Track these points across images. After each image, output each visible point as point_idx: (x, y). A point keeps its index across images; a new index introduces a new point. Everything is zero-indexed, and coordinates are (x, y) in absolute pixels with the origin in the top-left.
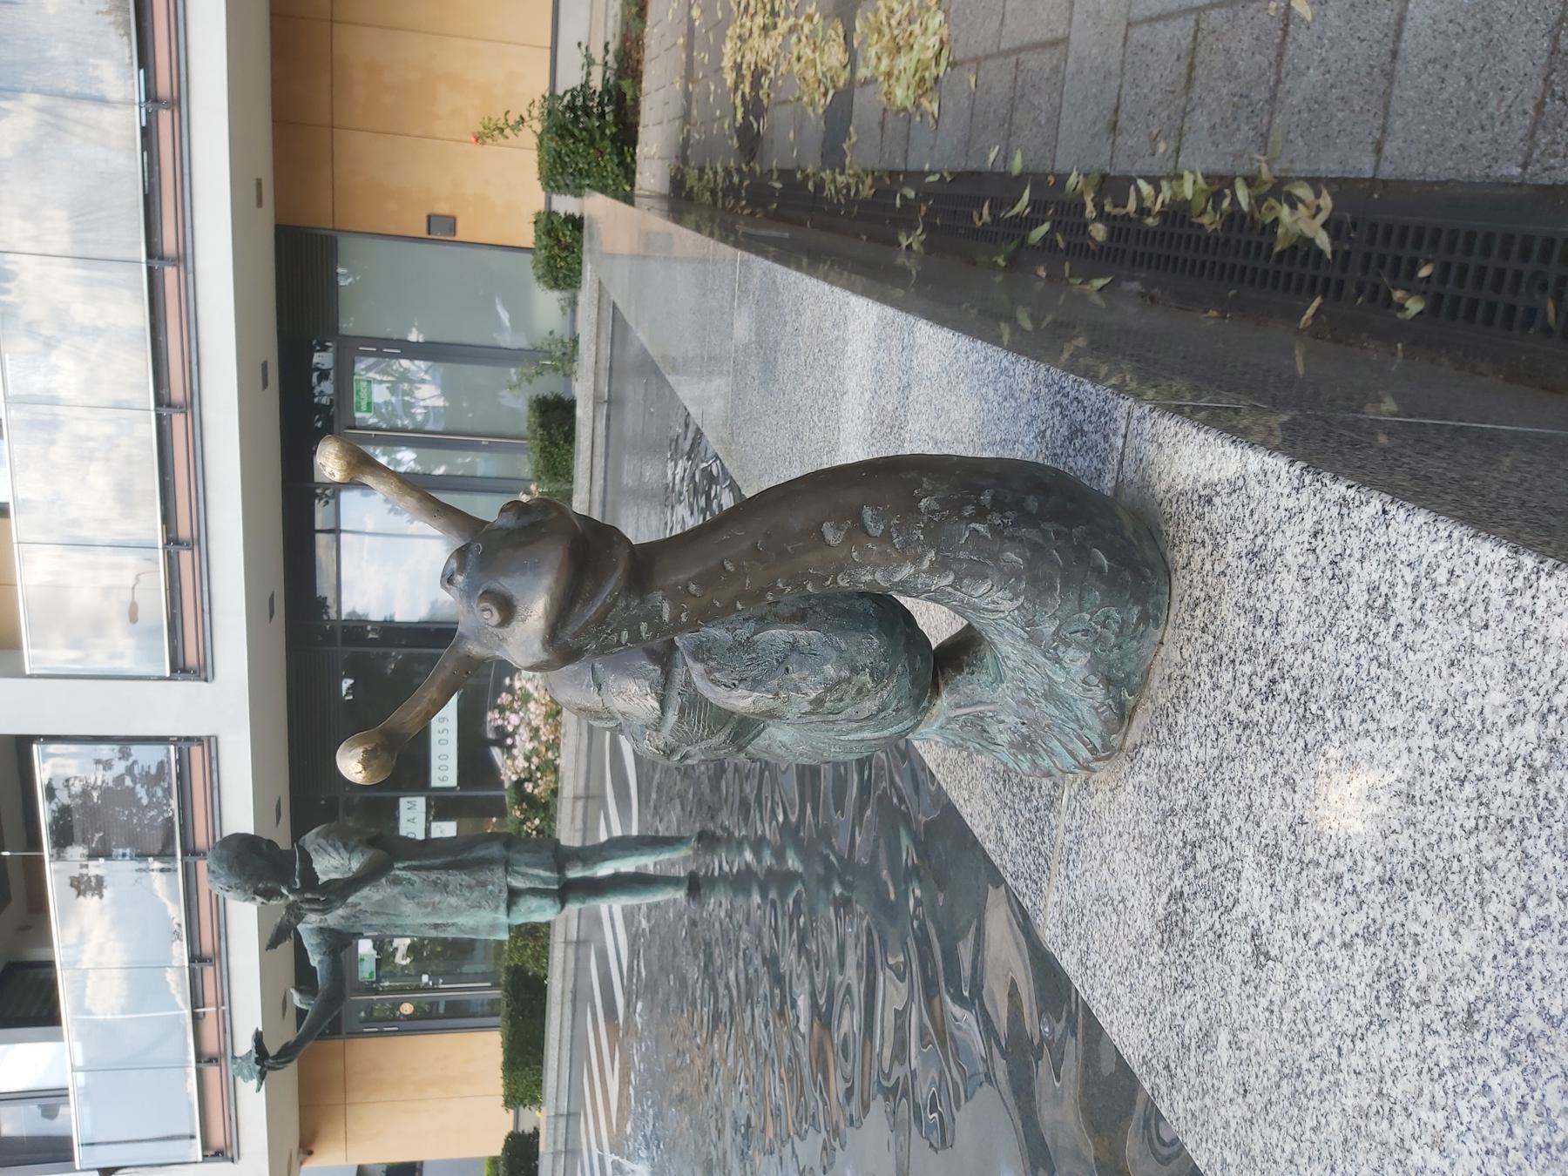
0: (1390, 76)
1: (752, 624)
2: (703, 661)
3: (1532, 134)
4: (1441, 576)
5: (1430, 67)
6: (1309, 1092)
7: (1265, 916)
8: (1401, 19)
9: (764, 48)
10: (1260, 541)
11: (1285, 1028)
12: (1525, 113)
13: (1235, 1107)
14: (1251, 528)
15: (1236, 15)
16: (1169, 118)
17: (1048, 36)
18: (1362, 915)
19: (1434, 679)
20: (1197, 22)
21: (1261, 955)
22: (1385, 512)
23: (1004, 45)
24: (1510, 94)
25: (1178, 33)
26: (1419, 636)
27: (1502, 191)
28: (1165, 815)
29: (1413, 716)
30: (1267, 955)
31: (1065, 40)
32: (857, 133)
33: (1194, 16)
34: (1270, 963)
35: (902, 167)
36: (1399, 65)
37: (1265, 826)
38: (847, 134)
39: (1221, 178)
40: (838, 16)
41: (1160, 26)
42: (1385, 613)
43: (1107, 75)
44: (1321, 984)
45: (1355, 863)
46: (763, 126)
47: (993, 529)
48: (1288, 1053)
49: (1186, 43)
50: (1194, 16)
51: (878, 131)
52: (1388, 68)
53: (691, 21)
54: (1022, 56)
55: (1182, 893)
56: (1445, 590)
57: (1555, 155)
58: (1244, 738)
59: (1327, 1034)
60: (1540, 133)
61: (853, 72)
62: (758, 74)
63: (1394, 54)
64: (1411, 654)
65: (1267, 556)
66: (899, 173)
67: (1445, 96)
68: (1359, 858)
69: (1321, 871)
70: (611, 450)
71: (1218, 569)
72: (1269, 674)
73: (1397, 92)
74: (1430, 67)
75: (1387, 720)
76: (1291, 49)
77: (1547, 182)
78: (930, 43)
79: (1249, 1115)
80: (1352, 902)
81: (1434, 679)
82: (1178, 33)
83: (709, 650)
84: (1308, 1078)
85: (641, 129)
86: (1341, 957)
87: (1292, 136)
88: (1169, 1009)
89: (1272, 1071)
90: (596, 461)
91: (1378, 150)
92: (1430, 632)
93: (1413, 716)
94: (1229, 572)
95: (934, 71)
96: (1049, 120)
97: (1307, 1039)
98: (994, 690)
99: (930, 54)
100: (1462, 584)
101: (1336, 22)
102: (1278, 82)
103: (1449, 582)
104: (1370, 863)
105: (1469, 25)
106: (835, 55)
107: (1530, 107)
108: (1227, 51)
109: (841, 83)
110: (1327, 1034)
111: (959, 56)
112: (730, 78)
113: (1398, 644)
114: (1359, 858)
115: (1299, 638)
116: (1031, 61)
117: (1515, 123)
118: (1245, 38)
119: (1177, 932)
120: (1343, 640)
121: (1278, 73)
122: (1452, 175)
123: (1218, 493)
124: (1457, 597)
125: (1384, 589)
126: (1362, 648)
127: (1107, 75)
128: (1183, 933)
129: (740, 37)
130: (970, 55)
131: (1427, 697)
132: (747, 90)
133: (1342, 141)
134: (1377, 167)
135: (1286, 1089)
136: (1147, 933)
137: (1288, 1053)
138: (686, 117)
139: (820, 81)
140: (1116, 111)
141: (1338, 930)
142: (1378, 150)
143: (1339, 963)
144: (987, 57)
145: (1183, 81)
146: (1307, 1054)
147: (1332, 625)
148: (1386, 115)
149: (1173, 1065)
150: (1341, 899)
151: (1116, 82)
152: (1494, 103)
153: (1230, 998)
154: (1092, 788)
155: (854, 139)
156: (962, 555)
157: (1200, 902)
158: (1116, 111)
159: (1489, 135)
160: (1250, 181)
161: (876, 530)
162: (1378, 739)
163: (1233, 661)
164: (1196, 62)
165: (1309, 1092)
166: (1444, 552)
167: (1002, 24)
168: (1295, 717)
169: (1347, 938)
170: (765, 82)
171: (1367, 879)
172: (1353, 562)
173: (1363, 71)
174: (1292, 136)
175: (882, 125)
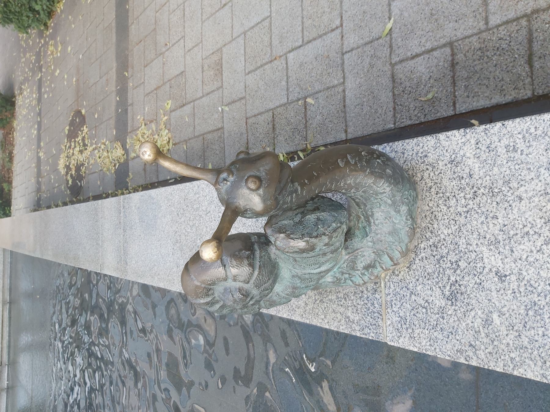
0: (345, 112)
1: (300, 215)
2: (284, 233)
3: (394, 116)
4: (532, 130)
5: (357, 107)
6: (542, 307)
7: (500, 263)
8: (344, 97)
9: (81, 158)
10: (454, 156)
11: (523, 294)
12: (390, 111)
13: (509, 336)
14: (448, 155)
15: (287, 108)
16: (268, 141)
17: (215, 128)
18: (542, 238)
19: (541, 158)
20: (273, 113)
21: (502, 277)
22: (503, 125)
23: (196, 134)
24: (385, 108)
25: (266, 117)
26: (531, 149)
27: (389, 132)
28: (438, 261)
29: (538, 171)
30: (506, 276)
31: (222, 128)
32: (132, 174)
33: (271, 111)
34: (508, 277)
35: (157, 181)
36: (347, 108)
37: (488, 236)
38: (128, 176)
39: (292, 152)
40: (117, 140)
41: (259, 116)
42: (515, 150)
43: (242, 134)
44: (533, 269)
45: (532, 224)
46: (83, 183)
47: (382, 161)
48: (527, 301)
49: (270, 119)
50: (271, 111)
51: (143, 172)
52: (343, 110)
53: (39, 158)
54: (205, 136)
55: (456, 281)
56: (535, 133)
57: (403, 119)
58: (468, 216)
59: (542, 284)
60: (397, 115)
61: (127, 156)
62: (78, 168)
63: (344, 106)
64: (530, 156)
65: (459, 159)
66: (155, 183)
67: (364, 112)
68: (533, 222)
69: (519, 236)
70: (12, 323)
71: (437, 173)
72: (473, 191)
73: (348, 115)
74: (357, 107)
75: (528, 178)
76: (309, 113)
77: (403, 126)
78: (165, 139)
79: (517, 334)
80: (536, 237)
81: (541, 158)
82: (266, 117)
83: (285, 228)
84: (539, 303)
85: (13, 200)
86: (539, 256)
87: (315, 135)
88: (464, 324)
89: (522, 312)
90: (4, 329)
91: (346, 131)
92: (534, 147)
93: (538, 171)
94: (442, 172)
95: (167, 147)
96: (220, 152)
97: (534, 291)
98: (362, 242)
99: (165, 142)
100: (541, 129)
101: (323, 102)
102: (306, 122)
103: (536, 131)
104: (538, 221)
105: (367, 94)
106: (119, 152)
107: (391, 109)
108: (286, 118)
109: (122, 161)
110: (542, 284)
111: (177, 141)
112: (63, 172)
113: (524, 155)
114: (533, 222)
115: (481, 174)
116: (209, 136)
117: (388, 114)
118: (292, 113)
119: (458, 295)
120: (502, 165)
121: (306, 120)
122: (372, 132)
123: (429, 153)
124: (541, 133)
125: (512, 144)
126: (509, 164)
127: (242, 134)
128: (462, 294)
129: (67, 157)
130: (182, 140)
131: (540, 163)
132: (73, 173)
133: (333, 132)
134: (346, 136)
135: (531, 313)
136: (443, 305)
137: (527, 301)
138: (39, 190)
139: (111, 162)
140: (247, 143)
141: (533, 248)
142: (346, 131)
143: (538, 258)
144: (190, 139)
145: (271, 129)
146: (536, 295)
147: (494, 164)
148: (346, 122)
149: (473, 343)
150: (531, 239)
151: (245, 136)
152: (380, 111)
153: (493, 301)
154: (397, 273)
155: (131, 177)
156: (376, 170)
157: (466, 278)
158: (247, 143)
159: (381, 119)
160: (303, 151)
161: (353, 162)
162: (527, 184)
163: (455, 196)
164: (275, 123)
165: (542, 307)
166: (531, 124)
167: (194, 128)
168: (489, 197)
169: (538, 248)
170: (83, 169)
171: (539, 226)
172: (496, 143)
173: (335, 112)
174: (315, 135)
175: (145, 170)
